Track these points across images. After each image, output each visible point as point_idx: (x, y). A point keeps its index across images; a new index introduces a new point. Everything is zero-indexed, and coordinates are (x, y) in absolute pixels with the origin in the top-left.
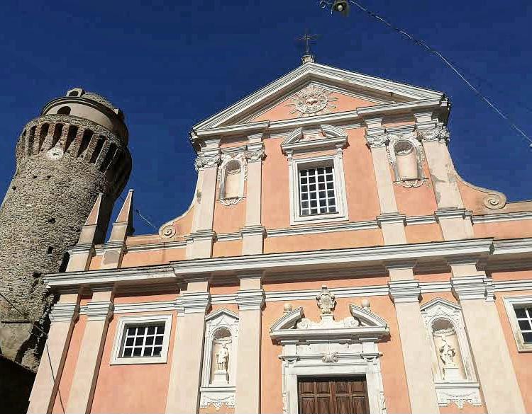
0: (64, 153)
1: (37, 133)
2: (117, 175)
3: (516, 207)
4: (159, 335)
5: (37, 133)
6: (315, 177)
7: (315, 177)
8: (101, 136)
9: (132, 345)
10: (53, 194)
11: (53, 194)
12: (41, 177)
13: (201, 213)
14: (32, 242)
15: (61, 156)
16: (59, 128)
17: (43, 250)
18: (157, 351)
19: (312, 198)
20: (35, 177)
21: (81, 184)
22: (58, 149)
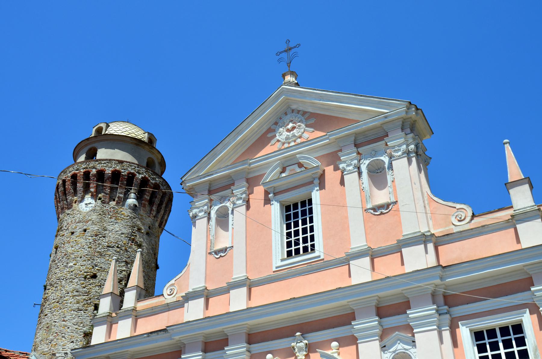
0: (96, 201)
1: (68, 185)
2: (154, 208)
3: (485, 219)
4: (306, 245)
5: (68, 185)
6: (297, 214)
7: (297, 214)
8: (130, 173)
9: (295, 249)
10: (91, 247)
11: (91, 247)
12: (78, 231)
13: (196, 273)
14: (78, 303)
15: (93, 205)
16: (87, 175)
17: (89, 308)
18: (313, 249)
19: (298, 239)
20: (73, 233)
21: (118, 230)
22: (88, 199)
